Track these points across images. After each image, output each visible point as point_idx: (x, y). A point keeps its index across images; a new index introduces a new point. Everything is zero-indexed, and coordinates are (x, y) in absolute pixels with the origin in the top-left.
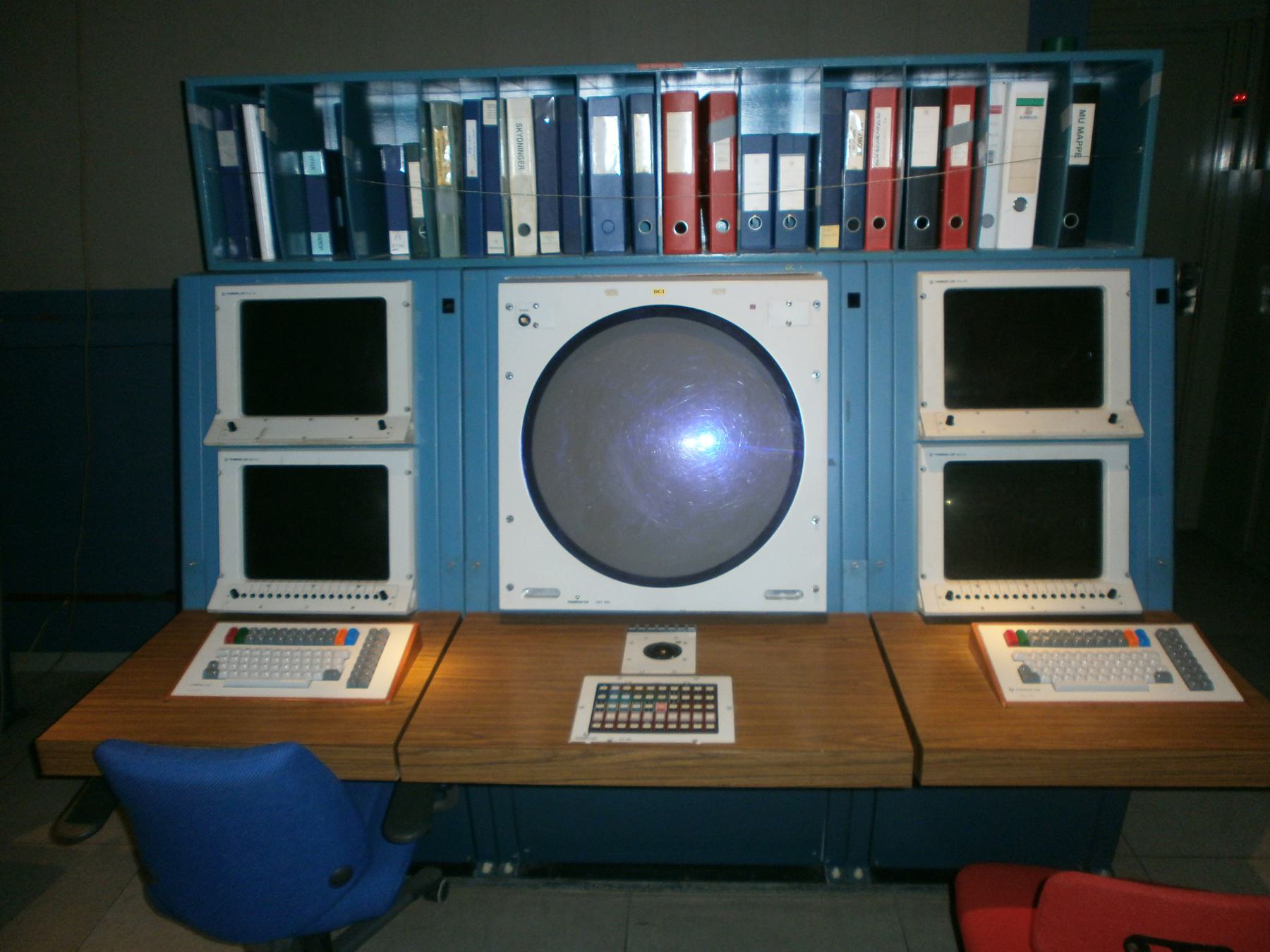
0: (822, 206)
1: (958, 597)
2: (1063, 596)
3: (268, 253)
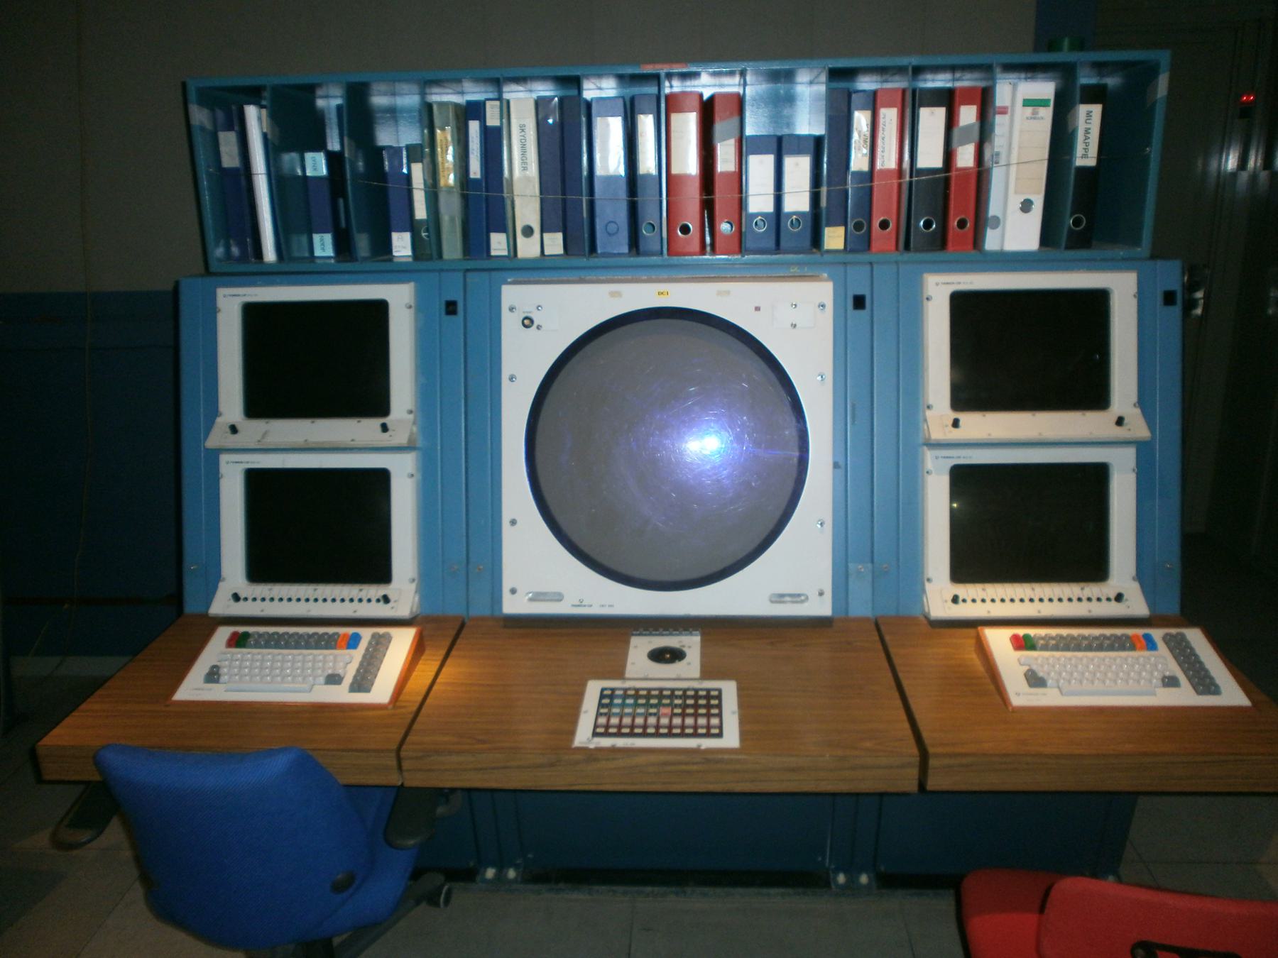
0: (827, 207)
1: (964, 601)
2: (1070, 600)
3: (270, 254)
